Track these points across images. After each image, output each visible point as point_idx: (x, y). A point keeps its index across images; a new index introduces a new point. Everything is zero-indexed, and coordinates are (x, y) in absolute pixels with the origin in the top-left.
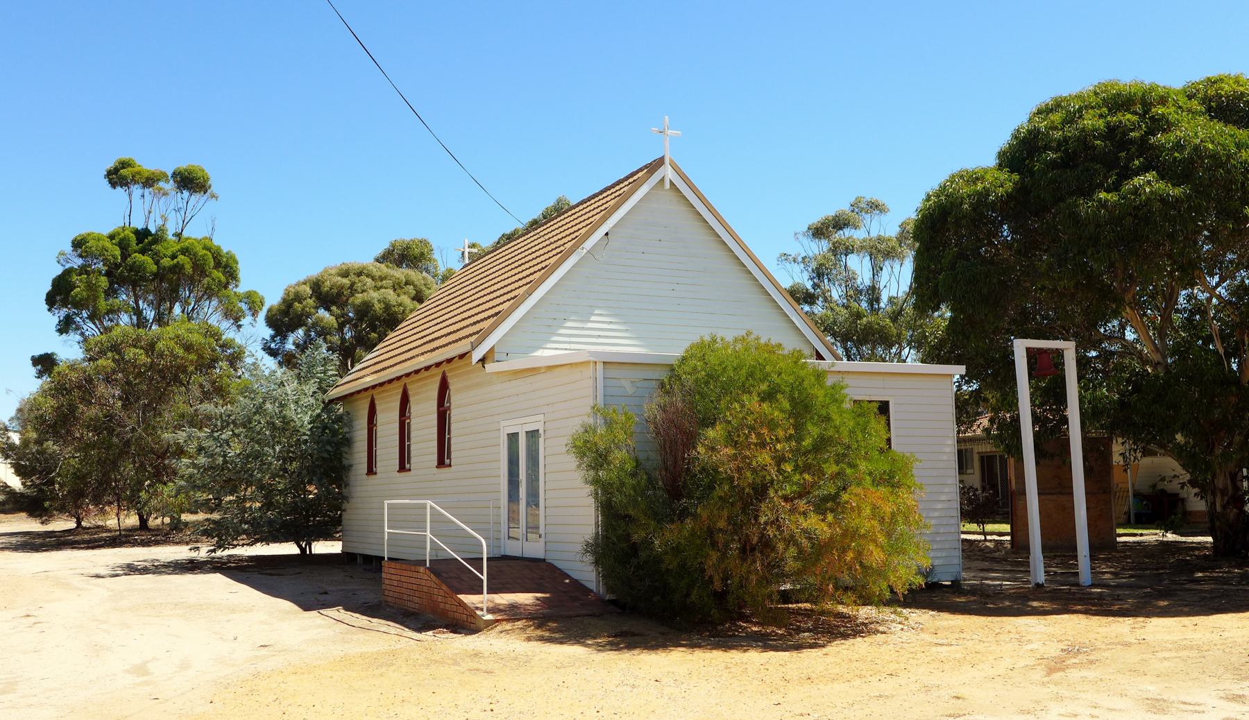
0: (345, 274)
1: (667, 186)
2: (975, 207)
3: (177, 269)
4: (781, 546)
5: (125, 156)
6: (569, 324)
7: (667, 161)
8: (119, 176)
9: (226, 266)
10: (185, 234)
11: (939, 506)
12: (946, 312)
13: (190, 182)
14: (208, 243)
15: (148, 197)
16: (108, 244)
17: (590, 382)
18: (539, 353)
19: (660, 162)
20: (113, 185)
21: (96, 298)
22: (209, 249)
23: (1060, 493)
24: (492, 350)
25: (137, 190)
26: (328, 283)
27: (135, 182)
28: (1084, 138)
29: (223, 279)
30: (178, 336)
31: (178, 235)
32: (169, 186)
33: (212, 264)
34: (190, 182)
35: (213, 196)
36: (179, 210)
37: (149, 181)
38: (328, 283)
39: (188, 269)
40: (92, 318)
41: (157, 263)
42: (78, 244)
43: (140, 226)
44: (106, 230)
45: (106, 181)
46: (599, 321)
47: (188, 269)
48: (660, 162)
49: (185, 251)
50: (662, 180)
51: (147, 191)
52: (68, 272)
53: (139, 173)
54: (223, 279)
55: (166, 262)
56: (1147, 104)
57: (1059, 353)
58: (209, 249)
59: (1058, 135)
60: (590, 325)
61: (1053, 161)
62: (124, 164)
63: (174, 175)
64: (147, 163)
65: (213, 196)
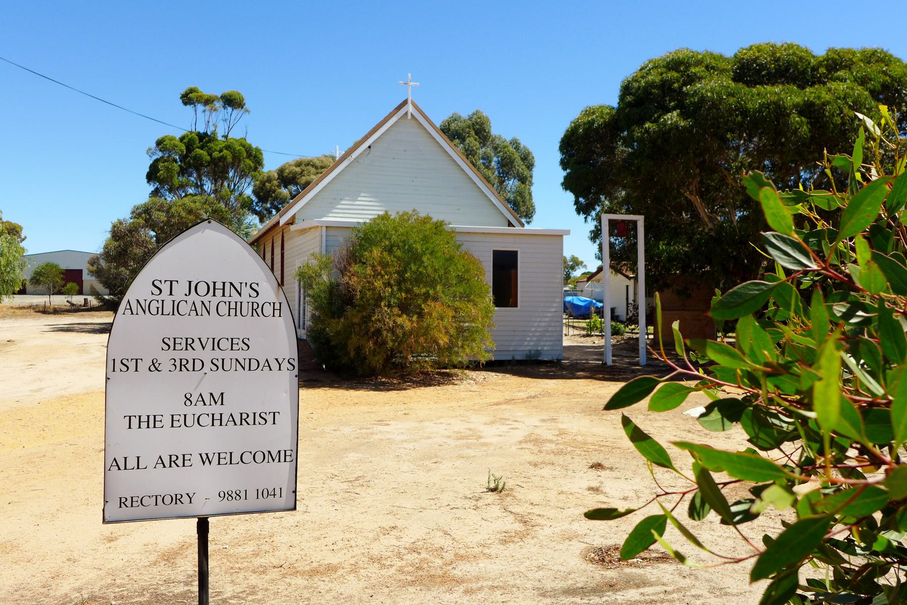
0: (299, 164)
1: (409, 117)
2: (585, 130)
3: (222, 159)
4: (385, 333)
5: (192, 86)
6: (343, 202)
7: (409, 102)
8: (188, 98)
9: (255, 157)
10: (230, 136)
11: (550, 315)
12: (602, 197)
13: (232, 102)
14: (243, 141)
15: (207, 113)
16: (178, 143)
17: (318, 238)
18: (324, 219)
19: (405, 103)
20: (185, 104)
21: (172, 177)
22: (244, 146)
23: (683, 310)
24: (294, 217)
25: (200, 107)
26: (287, 171)
27: (199, 102)
28: (652, 85)
29: (252, 165)
30: (184, 204)
31: (226, 137)
32: (218, 104)
33: (245, 155)
34: (232, 102)
35: (247, 111)
36: (226, 120)
37: (208, 101)
38: (287, 171)
39: (230, 159)
40: (170, 190)
41: (210, 155)
42: (159, 143)
43: (202, 130)
44: (178, 135)
45: (181, 101)
46: (363, 200)
47: (230, 159)
48: (405, 103)
49: (228, 147)
50: (406, 113)
51: (208, 108)
52: (156, 161)
53: (200, 96)
54: (252, 165)
55: (216, 154)
56: (688, 65)
57: (635, 223)
58: (244, 146)
59: (636, 85)
60: (357, 203)
61: (629, 102)
62: (192, 91)
63: (222, 97)
64: (206, 90)
65: (247, 111)
